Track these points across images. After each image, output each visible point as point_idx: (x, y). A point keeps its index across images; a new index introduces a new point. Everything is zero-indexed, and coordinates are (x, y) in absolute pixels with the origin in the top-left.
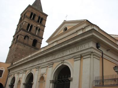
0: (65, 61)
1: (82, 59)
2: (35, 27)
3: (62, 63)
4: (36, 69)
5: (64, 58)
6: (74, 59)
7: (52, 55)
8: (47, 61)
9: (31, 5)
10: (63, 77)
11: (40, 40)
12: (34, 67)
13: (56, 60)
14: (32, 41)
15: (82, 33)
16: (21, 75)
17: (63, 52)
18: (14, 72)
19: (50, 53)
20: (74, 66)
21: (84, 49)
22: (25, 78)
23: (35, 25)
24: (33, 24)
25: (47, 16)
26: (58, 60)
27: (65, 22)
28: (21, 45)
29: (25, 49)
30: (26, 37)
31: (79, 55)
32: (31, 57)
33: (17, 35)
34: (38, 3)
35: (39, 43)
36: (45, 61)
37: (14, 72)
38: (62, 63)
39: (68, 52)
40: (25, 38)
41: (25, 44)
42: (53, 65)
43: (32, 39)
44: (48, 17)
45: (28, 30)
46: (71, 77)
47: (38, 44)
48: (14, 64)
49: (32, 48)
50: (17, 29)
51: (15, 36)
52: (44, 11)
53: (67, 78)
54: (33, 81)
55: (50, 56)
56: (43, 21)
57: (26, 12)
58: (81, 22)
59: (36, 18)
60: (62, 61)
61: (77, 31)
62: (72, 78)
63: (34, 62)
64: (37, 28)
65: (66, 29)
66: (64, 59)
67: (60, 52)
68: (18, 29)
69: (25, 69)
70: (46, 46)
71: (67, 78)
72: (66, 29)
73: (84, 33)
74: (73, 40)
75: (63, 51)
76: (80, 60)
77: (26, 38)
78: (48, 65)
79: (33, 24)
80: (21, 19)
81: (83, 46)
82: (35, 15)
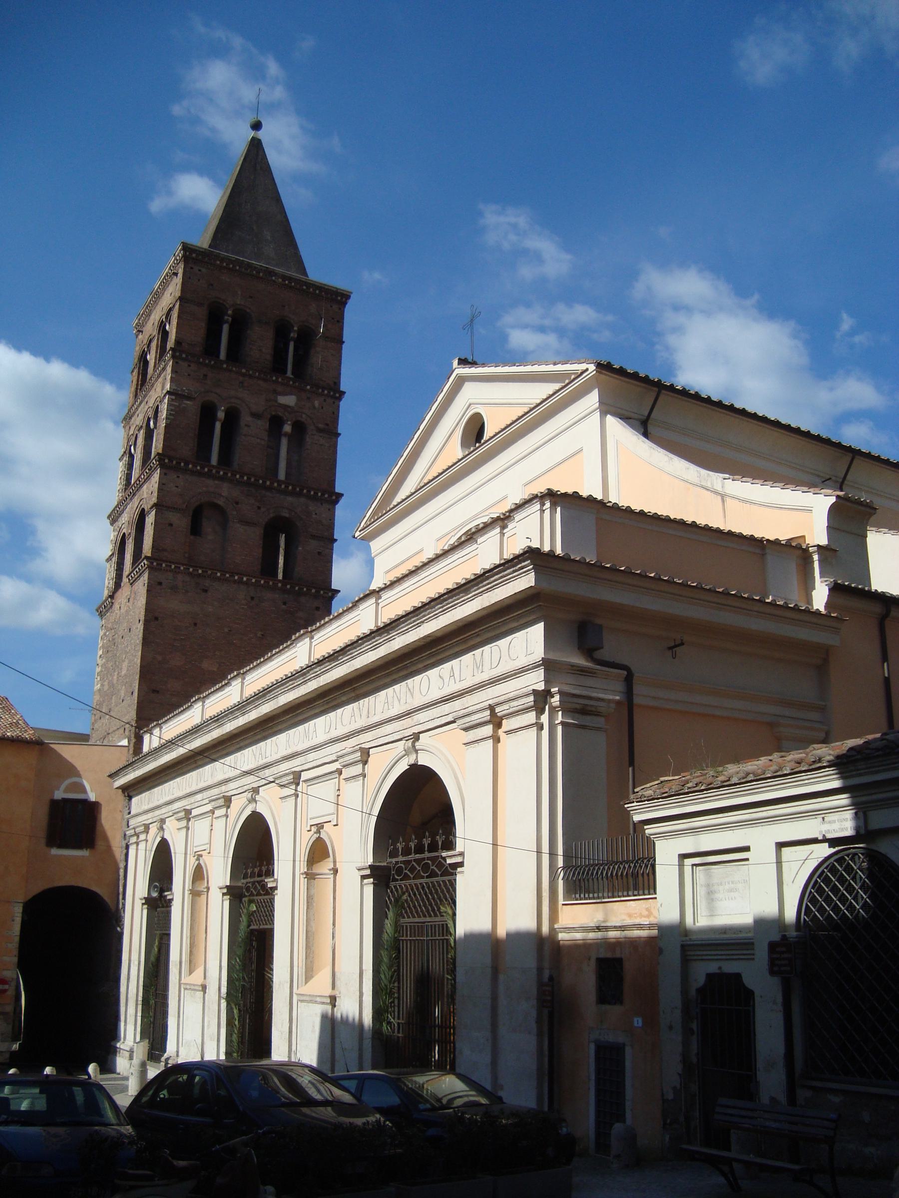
2: (256, 416)
3: (407, 753)
9: (202, 240)
16: (318, 801)
25: (337, 299)
28: (174, 588)
31: (527, 695)
35: (314, 537)
38: (407, 753)
40: (195, 529)
42: (365, 763)
45: (208, 459)
56: (317, 358)
59: (260, 344)
62: (462, 854)
64: (276, 422)
66: (416, 730)
68: (131, 457)
77: (209, 527)
82: (240, 324)
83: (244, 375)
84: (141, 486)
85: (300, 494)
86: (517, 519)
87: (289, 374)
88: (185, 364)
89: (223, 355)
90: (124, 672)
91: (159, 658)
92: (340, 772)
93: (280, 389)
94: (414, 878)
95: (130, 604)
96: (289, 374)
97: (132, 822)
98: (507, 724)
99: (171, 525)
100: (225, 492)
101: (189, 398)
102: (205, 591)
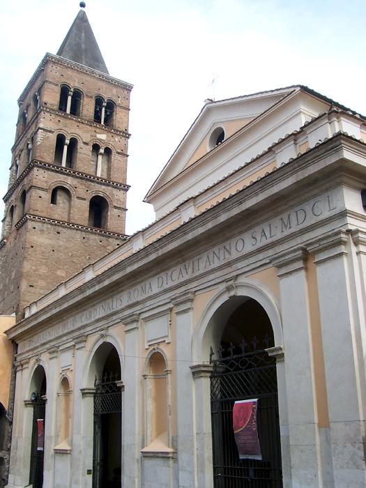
0: (242, 280)
1: (311, 264)
2: (86, 143)
3: (229, 289)
4: (126, 324)
5: (234, 267)
6: (280, 267)
7: (184, 261)
8: (166, 286)
10: (243, 346)
11: (118, 194)
12: (114, 318)
13: (201, 281)
14: (85, 205)
15: (295, 157)
17: (227, 244)
18: (36, 348)
19: (174, 252)
20: (286, 302)
21: (313, 222)
22: (87, 361)
23: (84, 134)
24: (78, 131)
25: (127, 88)
26: (211, 277)
27: (211, 108)
28: (42, 231)
29: (61, 243)
30: (56, 192)
31: (295, 251)
32: (98, 279)
33: (19, 190)
34: (81, 43)
35: (115, 207)
36: (155, 290)
37: (36, 348)
39: (247, 243)
40: (53, 201)
41: (60, 223)
43: (85, 199)
44: (132, 94)
46: (276, 345)
47: (112, 213)
48: (27, 315)
49: (92, 237)
50: (15, 164)
51: (13, 197)
52: (116, 69)
53: (260, 351)
54: (119, 378)
55: (176, 264)
56: (118, 115)
57: (37, 86)
58: (281, 100)
59: (88, 107)
60: (227, 281)
61: (270, 149)
63: (112, 297)
64: (96, 148)
65: (218, 137)
66: (235, 274)
67: (214, 246)
69: (79, 329)
70: (150, 226)
71: (260, 351)
72: (218, 137)
73: (302, 155)
74: (263, 189)
75: (228, 239)
76: (306, 269)
77: (61, 198)
78: (171, 305)
79: (78, 131)
80: (23, 117)
81: (307, 207)
82: (77, 95)
83: (79, 122)
84: (23, 179)
85: (108, 185)
86: (308, 132)
87: (102, 123)
88: (48, 114)
89: (68, 111)
90: (13, 277)
91: (34, 268)
92: (74, 346)
93: (97, 130)
94: (257, 366)
95: (16, 241)
96: (102, 123)
97: (18, 359)
98: (24, 367)
99: (40, 197)
100: (69, 182)
101: (50, 132)
102: (59, 233)
